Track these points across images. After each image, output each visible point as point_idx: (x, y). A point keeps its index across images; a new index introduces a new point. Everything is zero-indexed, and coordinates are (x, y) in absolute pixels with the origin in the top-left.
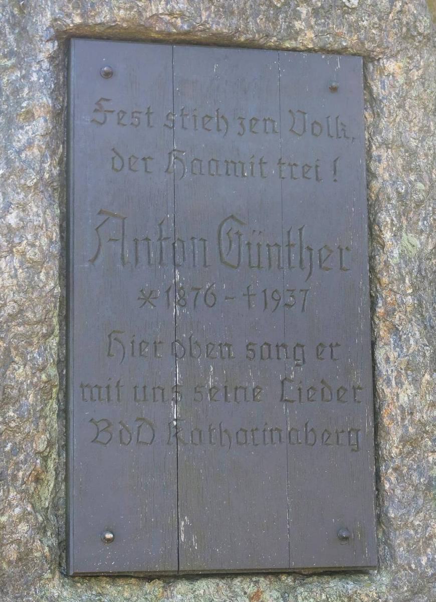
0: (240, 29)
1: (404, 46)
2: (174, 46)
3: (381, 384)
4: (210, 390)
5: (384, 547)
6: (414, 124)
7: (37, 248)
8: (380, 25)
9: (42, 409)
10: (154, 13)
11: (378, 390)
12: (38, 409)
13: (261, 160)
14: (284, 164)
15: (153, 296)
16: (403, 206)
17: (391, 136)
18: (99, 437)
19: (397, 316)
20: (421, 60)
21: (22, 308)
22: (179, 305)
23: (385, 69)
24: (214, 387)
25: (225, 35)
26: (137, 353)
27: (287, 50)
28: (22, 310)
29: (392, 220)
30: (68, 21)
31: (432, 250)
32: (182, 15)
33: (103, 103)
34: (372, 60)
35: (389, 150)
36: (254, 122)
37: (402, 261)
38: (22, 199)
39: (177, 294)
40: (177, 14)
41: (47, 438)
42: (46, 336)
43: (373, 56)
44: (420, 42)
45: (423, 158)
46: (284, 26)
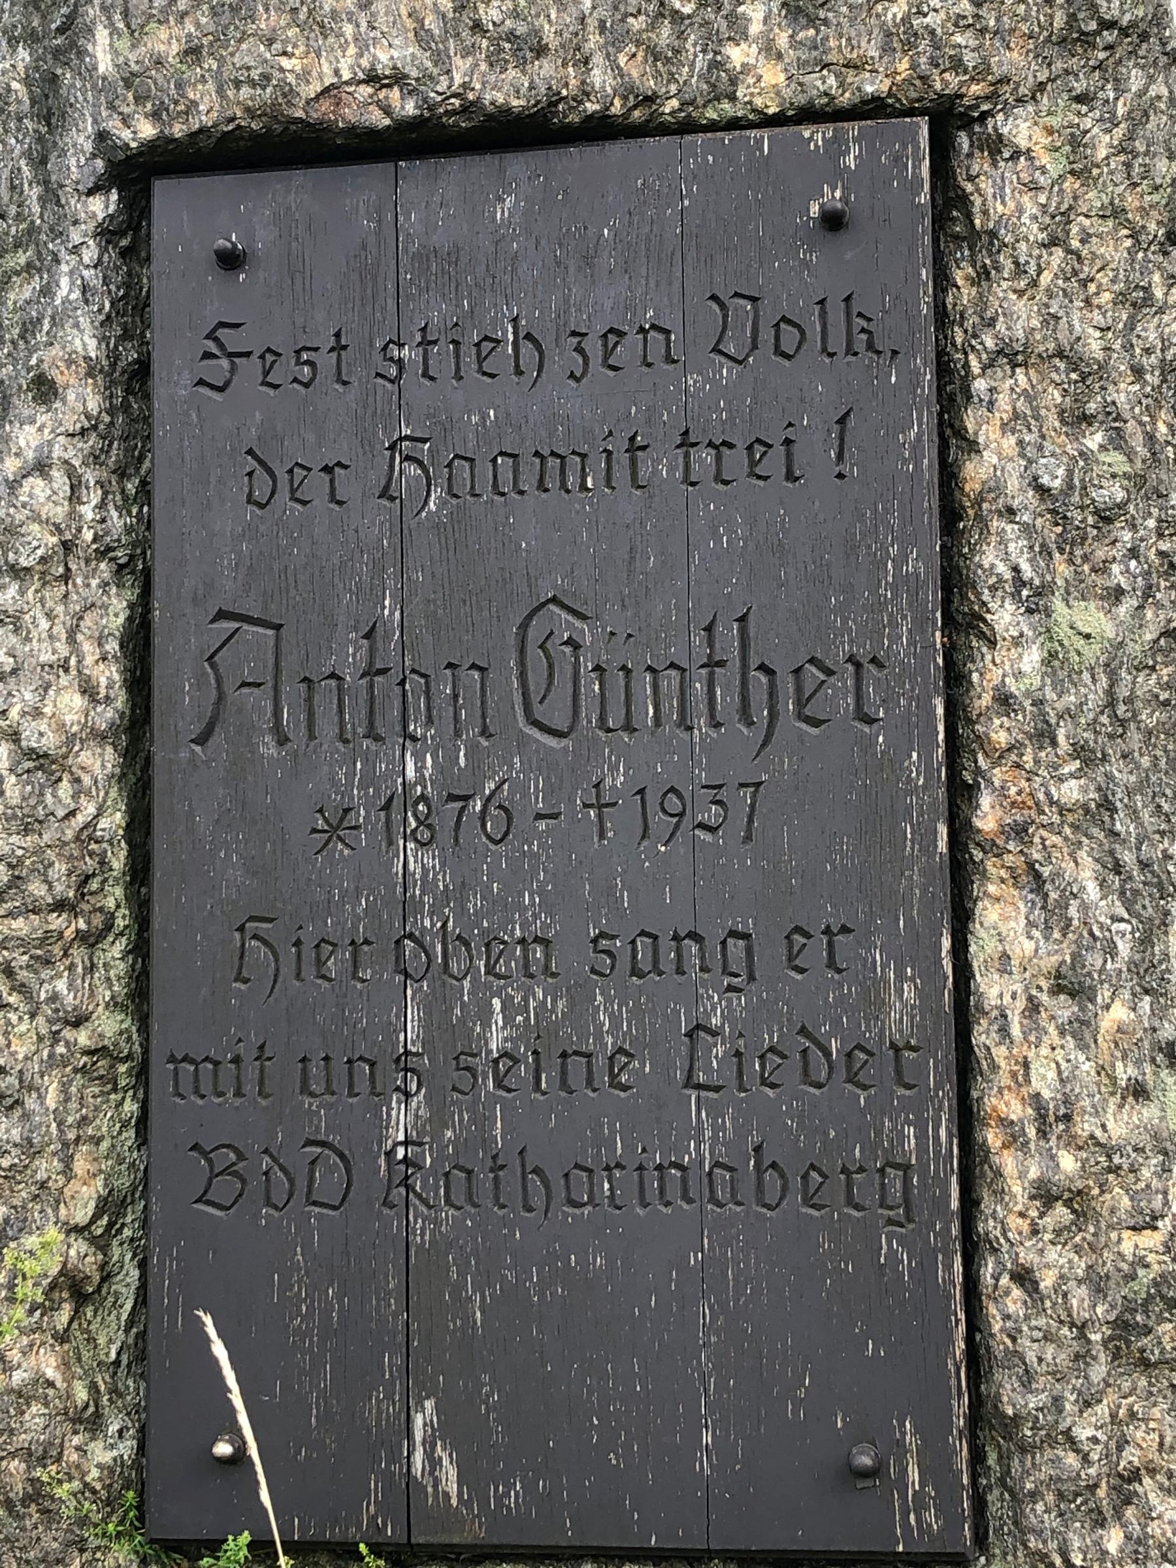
0: (564, 92)
1: (1059, 66)
2: (402, 164)
3: (983, 1036)
4: (496, 1061)
5: (1002, 1494)
6: (1099, 286)
7: (45, 720)
8: (977, 16)
9: (84, 1121)
10: (327, 84)
11: (976, 1049)
12: (70, 1120)
13: (632, 439)
14: (696, 444)
15: (349, 822)
16: (1057, 524)
17: (1021, 331)
18: (210, 1191)
19: (1037, 840)
20: (1117, 99)
21: (16, 873)
22: (416, 840)
23: (1001, 142)
24: (505, 1054)
25: (520, 113)
26: (309, 972)
27: (713, 127)
28: (19, 878)
29: (1016, 569)
30: (126, 135)
31: (1156, 641)
32: (398, 78)
33: (222, 333)
34: (967, 122)
35: (1018, 370)
36: (612, 338)
37: (1048, 681)
38: (11, 602)
39: (409, 814)
40: (386, 77)
41: (98, 1192)
42: (90, 940)
43: (962, 109)
44: (1109, 47)
45: (1129, 380)
46: (701, 63)
